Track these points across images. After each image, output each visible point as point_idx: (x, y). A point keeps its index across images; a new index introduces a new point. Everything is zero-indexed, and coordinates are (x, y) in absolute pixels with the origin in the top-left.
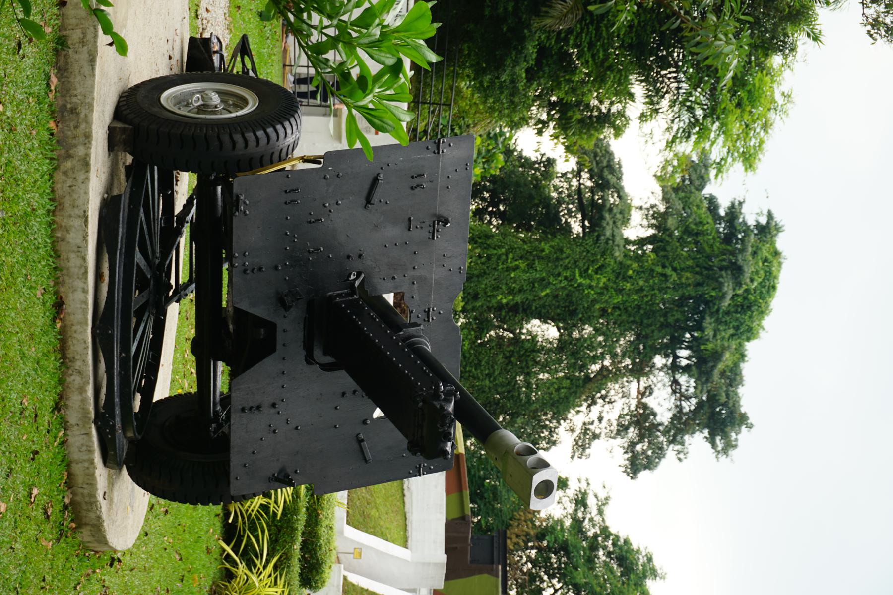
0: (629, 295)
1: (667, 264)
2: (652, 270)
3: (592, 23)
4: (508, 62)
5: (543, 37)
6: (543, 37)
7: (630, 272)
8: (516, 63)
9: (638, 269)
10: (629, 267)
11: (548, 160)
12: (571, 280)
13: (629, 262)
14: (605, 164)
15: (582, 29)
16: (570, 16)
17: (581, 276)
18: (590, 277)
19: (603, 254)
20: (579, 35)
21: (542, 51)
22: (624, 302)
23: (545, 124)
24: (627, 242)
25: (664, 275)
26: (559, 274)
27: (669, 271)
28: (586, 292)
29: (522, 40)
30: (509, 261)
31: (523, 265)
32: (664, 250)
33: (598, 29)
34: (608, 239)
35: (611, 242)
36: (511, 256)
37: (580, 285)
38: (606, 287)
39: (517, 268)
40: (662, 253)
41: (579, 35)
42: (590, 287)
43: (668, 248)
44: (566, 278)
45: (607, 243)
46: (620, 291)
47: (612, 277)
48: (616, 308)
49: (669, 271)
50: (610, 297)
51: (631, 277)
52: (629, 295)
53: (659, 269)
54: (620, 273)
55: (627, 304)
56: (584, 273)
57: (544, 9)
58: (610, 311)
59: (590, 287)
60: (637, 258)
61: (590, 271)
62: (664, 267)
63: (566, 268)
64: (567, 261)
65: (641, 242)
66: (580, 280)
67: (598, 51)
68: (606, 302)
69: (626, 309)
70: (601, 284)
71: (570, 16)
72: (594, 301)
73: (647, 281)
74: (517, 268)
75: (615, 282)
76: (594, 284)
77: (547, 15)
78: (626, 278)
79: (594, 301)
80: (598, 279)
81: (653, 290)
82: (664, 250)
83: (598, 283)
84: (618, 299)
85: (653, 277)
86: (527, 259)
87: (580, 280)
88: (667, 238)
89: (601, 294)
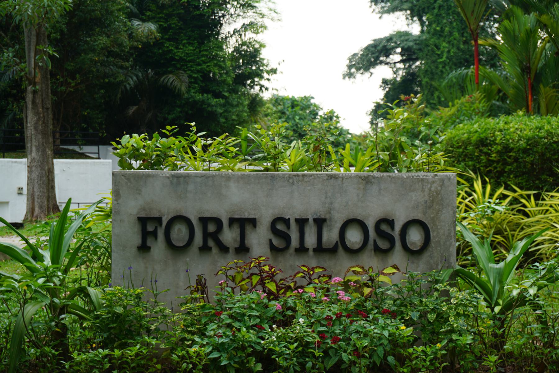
0: (454, 28)
1: (432, 6)
2: (437, 15)
3: (186, 65)
4: (209, 109)
5: (193, 91)
6: (193, 91)
7: (438, 28)
8: (209, 105)
9: (436, 24)
10: (435, 30)
11: (383, 83)
12: (445, 64)
13: (432, 30)
14: (373, 49)
15: (189, 70)
16: (181, 77)
17: (442, 58)
18: (442, 52)
19: (427, 46)
20: (192, 71)
21: (203, 91)
22: (459, 31)
23: (262, 86)
24: (422, 31)
25: (440, 7)
26: (442, 71)
27: (436, 5)
28: (452, 54)
29: (195, 102)
30: (434, 102)
31: (436, 94)
32: (424, 9)
33: (189, 61)
34: (416, 44)
35: (417, 42)
36: (432, 101)
37: (447, 58)
38: (449, 42)
39: (439, 97)
40: (426, 10)
41: (192, 71)
42: (449, 52)
43: (423, 6)
44: (444, 67)
45: (418, 44)
46: (451, 33)
47: (442, 39)
48: (462, 35)
49: (436, 5)
50: (455, 39)
51: (442, 28)
52: (454, 28)
53: (436, 11)
54: (440, 34)
55: (460, 29)
56: (440, 56)
57: (177, 91)
58: (464, 39)
59: (449, 52)
60: (430, 25)
61: (439, 53)
62: (434, 8)
63: (437, 68)
64: (433, 67)
65: (422, 24)
66: (444, 58)
67: (201, 60)
68: (458, 41)
69: (463, 29)
70: (447, 45)
71: (181, 77)
72: (458, 48)
73: (443, 18)
74: (439, 97)
75: (445, 37)
76: (446, 50)
77: (180, 90)
78: (442, 30)
79: (458, 48)
80: (444, 47)
81: (449, 13)
82: (424, 9)
83: (446, 47)
84: (456, 34)
85: (441, 14)
86: (433, 91)
87: (444, 58)
88: (417, 8)
89: (453, 45)
